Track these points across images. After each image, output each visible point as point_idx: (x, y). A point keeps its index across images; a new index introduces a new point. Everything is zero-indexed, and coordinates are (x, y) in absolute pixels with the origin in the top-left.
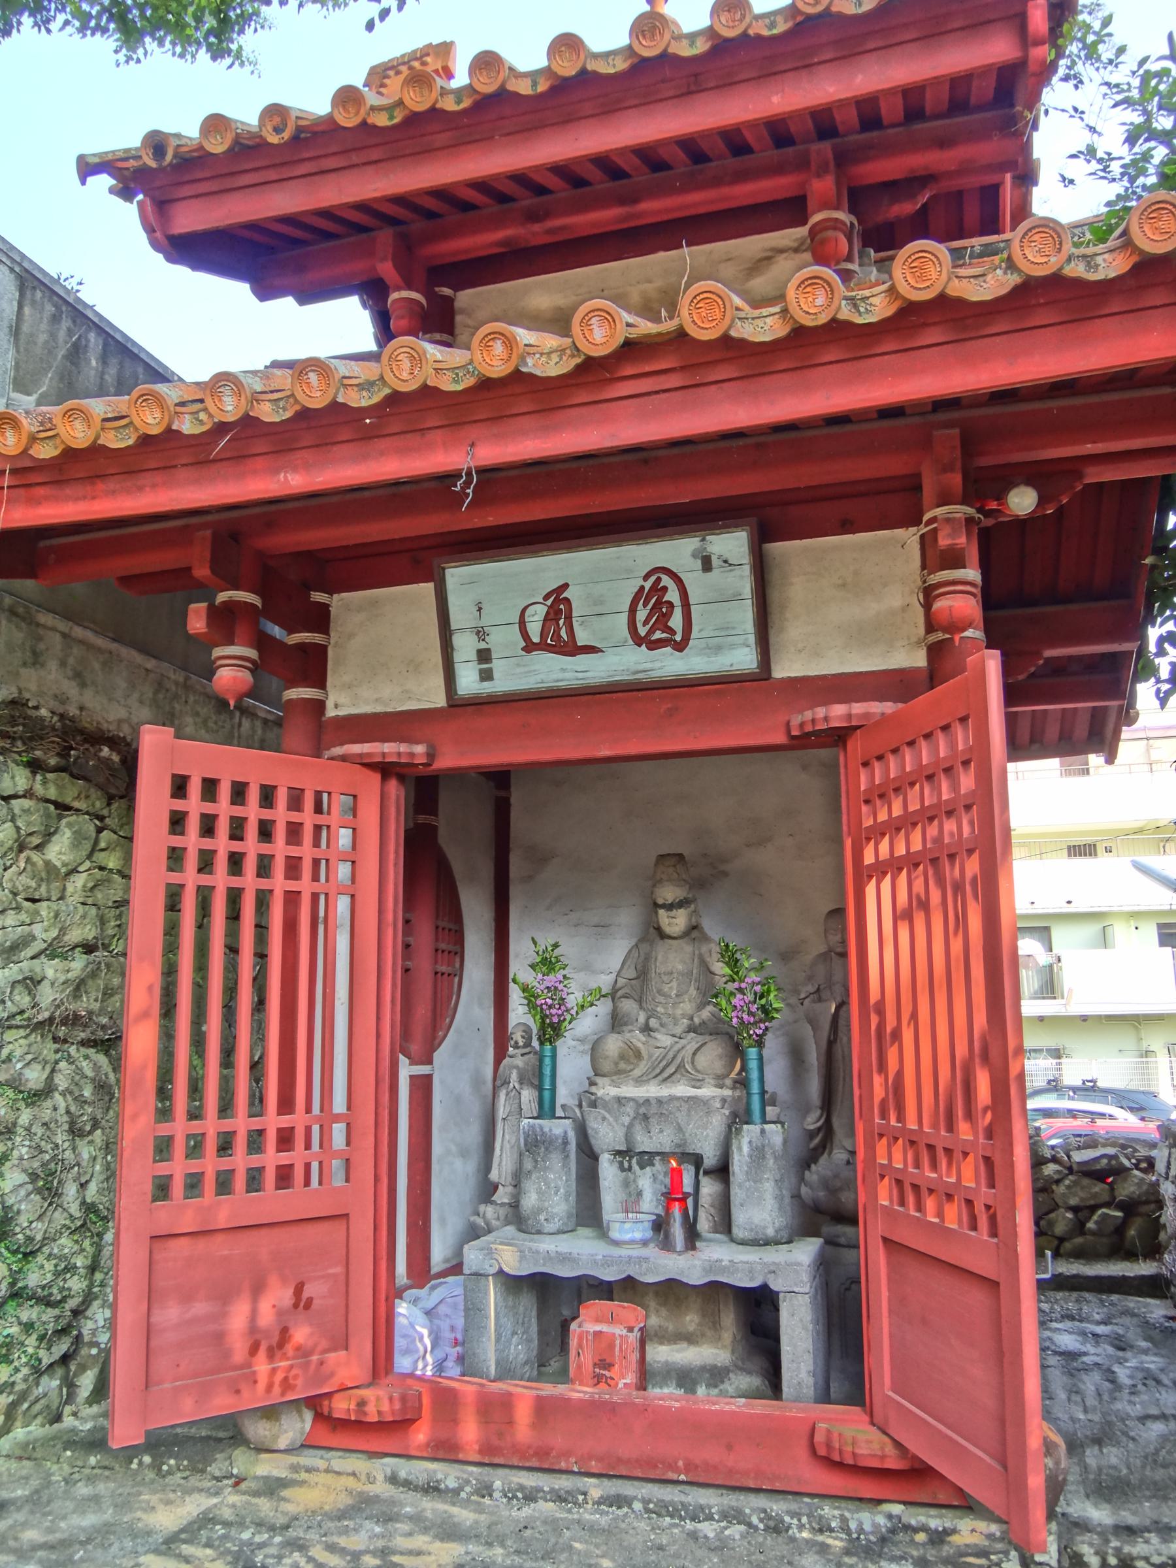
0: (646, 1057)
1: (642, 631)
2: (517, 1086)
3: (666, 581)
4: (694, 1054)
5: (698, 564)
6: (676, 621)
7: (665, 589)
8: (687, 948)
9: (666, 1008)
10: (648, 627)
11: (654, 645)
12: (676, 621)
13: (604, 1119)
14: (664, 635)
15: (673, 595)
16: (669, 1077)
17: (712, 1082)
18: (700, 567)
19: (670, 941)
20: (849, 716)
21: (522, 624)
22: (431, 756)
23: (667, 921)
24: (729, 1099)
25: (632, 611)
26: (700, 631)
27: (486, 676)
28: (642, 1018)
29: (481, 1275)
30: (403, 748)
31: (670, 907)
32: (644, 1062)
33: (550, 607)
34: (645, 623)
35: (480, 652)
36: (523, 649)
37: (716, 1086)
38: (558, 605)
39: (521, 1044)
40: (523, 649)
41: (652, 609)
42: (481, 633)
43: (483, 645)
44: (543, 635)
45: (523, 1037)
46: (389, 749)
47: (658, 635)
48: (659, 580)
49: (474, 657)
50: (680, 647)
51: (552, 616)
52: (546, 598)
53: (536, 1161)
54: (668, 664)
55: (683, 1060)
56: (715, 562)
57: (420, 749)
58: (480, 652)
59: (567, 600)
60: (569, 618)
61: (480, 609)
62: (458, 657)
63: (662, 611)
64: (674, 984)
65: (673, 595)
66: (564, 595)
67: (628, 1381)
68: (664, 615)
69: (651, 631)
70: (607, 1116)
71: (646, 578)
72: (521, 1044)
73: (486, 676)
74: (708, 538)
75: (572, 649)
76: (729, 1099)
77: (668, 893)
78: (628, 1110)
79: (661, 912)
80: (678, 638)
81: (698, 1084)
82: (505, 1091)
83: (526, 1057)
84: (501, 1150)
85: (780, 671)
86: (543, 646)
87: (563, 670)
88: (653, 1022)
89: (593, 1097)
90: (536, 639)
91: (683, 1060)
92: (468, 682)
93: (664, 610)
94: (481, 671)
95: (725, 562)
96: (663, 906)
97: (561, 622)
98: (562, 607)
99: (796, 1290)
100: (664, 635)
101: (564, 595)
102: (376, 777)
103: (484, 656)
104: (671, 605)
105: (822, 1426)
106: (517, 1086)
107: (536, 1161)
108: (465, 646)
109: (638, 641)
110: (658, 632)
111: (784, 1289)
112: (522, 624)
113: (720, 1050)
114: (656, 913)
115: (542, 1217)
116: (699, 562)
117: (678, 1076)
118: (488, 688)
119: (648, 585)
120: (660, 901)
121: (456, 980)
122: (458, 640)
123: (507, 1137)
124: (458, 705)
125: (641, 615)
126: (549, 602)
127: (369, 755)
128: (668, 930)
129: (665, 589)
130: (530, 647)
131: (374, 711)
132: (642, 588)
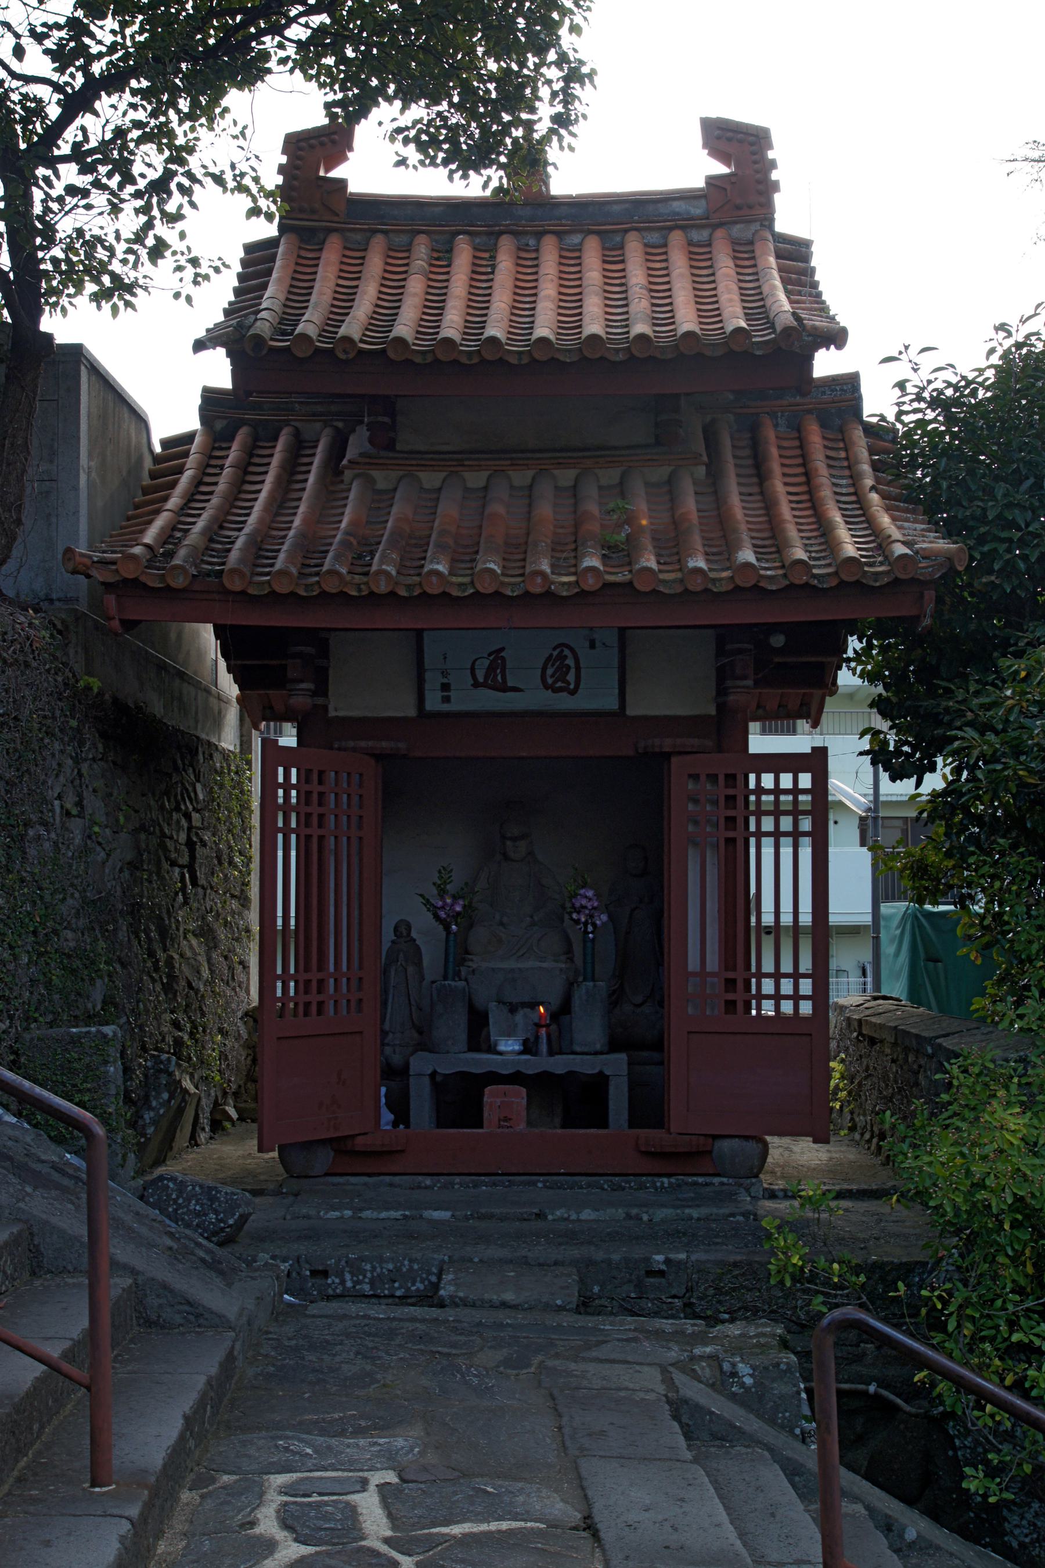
1: (550, 681)
3: (567, 652)
5: (587, 644)
6: (571, 677)
7: (566, 657)
11: (556, 690)
12: (571, 677)
15: (570, 661)
25: (544, 670)
27: (447, 700)
28: (498, 917)
31: (514, 839)
34: (552, 676)
38: (497, 661)
42: (444, 673)
43: (445, 681)
44: (486, 677)
47: (559, 684)
49: (439, 687)
50: (573, 693)
51: (491, 670)
52: (490, 655)
54: (565, 702)
56: (598, 644)
57: (401, 745)
59: (503, 659)
62: (427, 686)
65: (570, 661)
69: (555, 682)
75: (504, 688)
79: (509, 843)
85: (630, 712)
86: (484, 685)
88: (505, 920)
90: (481, 680)
92: (433, 702)
103: (446, 687)
104: (569, 667)
108: (433, 681)
109: (546, 687)
119: (555, 653)
122: (428, 675)
125: (550, 672)
129: (566, 657)
130: (476, 685)
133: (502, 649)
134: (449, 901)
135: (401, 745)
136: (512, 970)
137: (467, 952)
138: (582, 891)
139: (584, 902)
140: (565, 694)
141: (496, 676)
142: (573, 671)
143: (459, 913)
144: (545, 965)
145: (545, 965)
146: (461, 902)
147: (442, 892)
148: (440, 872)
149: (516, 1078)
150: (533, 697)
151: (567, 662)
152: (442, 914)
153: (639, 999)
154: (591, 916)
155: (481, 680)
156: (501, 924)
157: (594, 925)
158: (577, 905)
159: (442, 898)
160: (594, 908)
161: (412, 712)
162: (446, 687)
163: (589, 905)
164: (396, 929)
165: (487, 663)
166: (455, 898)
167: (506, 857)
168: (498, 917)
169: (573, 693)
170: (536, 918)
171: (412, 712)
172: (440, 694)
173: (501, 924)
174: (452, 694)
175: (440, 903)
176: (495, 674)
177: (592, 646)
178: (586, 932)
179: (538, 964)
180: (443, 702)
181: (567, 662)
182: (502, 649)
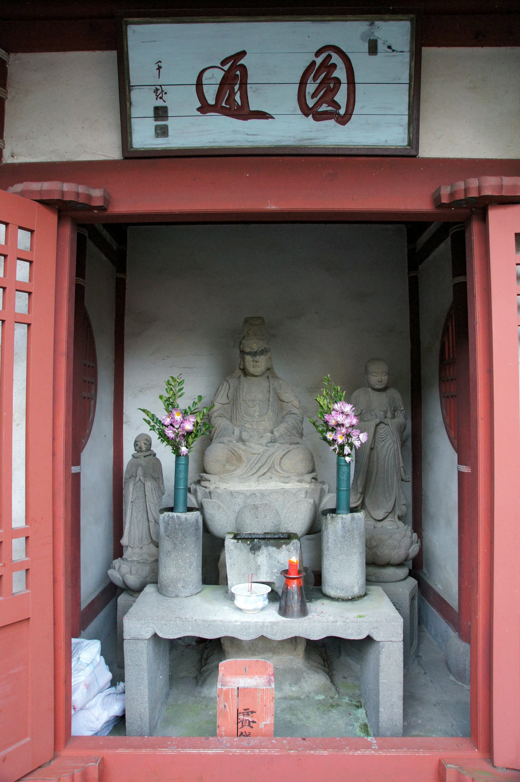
0: (245, 461)
1: (311, 103)
2: (141, 478)
3: (336, 59)
4: (281, 458)
5: (365, 47)
6: (341, 97)
7: (334, 66)
8: (265, 383)
9: (252, 425)
10: (316, 100)
11: (319, 116)
12: (341, 97)
13: (219, 507)
14: (330, 108)
15: (340, 73)
16: (264, 474)
17: (296, 478)
18: (367, 51)
19: (254, 378)
20: (501, 187)
21: (199, 85)
22: (107, 200)
23: (252, 364)
24: (309, 491)
25: (303, 83)
26: (363, 107)
27: (162, 132)
28: (237, 432)
29: (139, 639)
30: (81, 189)
31: (254, 354)
32: (245, 464)
33: (227, 72)
34: (313, 96)
35: (156, 109)
36: (198, 109)
37: (299, 481)
38: (235, 72)
39: (144, 449)
40: (198, 109)
41: (320, 84)
42: (159, 92)
43: (160, 103)
44: (219, 96)
45: (145, 444)
46: (68, 189)
47: (324, 108)
48: (329, 57)
49: (151, 113)
50: (343, 120)
51: (226, 82)
52: (223, 63)
53: (175, 544)
54: (330, 135)
55: (273, 463)
56: (381, 47)
57: (97, 193)
58: (156, 109)
59: (243, 68)
60: (244, 85)
61: (159, 68)
62: (135, 112)
63: (329, 86)
64: (257, 408)
65: (340, 73)
66: (242, 62)
67: (268, 723)
68: (332, 90)
69: (318, 104)
70: (222, 505)
71: (318, 54)
72: (144, 449)
73: (162, 132)
74: (377, 23)
75: (243, 112)
76: (309, 491)
77: (253, 345)
78: (239, 501)
79: (248, 358)
80: (342, 112)
81: (287, 480)
82: (132, 483)
83: (147, 458)
84: (130, 523)
85: (429, 149)
86: (216, 108)
87: (235, 132)
88: (245, 435)
89: (207, 490)
90: (211, 101)
91: (273, 463)
92: (144, 137)
93: (332, 86)
94: (157, 127)
95: (389, 47)
96: (250, 354)
97: (237, 87)
98: (238, 73)
99: (392, 639)
100: (330, 108)
101: (242, 62)
102: (52, 218)
103: (161, 113)
104: (338, 82)
105: (450, 767)
106: (141, 478)
107: (175, 544)
108: (142, 104)
109: (306, 111)
110: (324, 105)
111: (383, 639)
112: (199, 85)
113: (301, 456)
114: (243, 359)
115: (180, 585)
116: (367, 45)
117: (269, 474)
118: (161, 144)
119: (319, 61)
120: (248, 350)
121: (93, 402)
122: (135, 96)
123: (135, 514)
124: (133, 157)
125: (311, 88)
126: (226, 68)
127: (48, 192)
128: (252, 370)
129: (334, 66)
130: (205, 108)
131: (49, 160)
132: (314, 63)
133: (243, 54)
134: (178, 417)
135: (97, 193)
136: (253, 494)
137: (205, 472)
138: (337, 406)
139: (340, 419)
140: (332, 123)
141: (232, 94)
142: (344, 88)
143: (189, 433)
144: (288, 486)
145: (288, 486)
146: (192, 419)
147: (170, 405)
148: (169, 384)
149: (262, 645)
150: (287, 127)
151: (335, 74)
152: (170, 433)
153: (380, 514)
154: (348, 436)
155: (211, 101)
156: (241, 440)
157: (351, 445)
158: (332, 422)
159: (170, 413)
160: (352, 426)
161: (112, 152)
162: (161, 113)
163: (347, 423)
164: (136, 445)
165: (219, 75)
166: (185, 413)
167: (245, 372)
168: (237, 432)
169: (343, 120)
170: (276, 434)
171: (112, 152)
172: (151, 124)
173: (241, 440)
174: (171, 123)
175: (168, 421)
176: (231, 93)
177: (373, 49)
178: (341, 454)
179: (282, 485)
180: (157, 135)
181: (335, 74)
182: (243, 54)
